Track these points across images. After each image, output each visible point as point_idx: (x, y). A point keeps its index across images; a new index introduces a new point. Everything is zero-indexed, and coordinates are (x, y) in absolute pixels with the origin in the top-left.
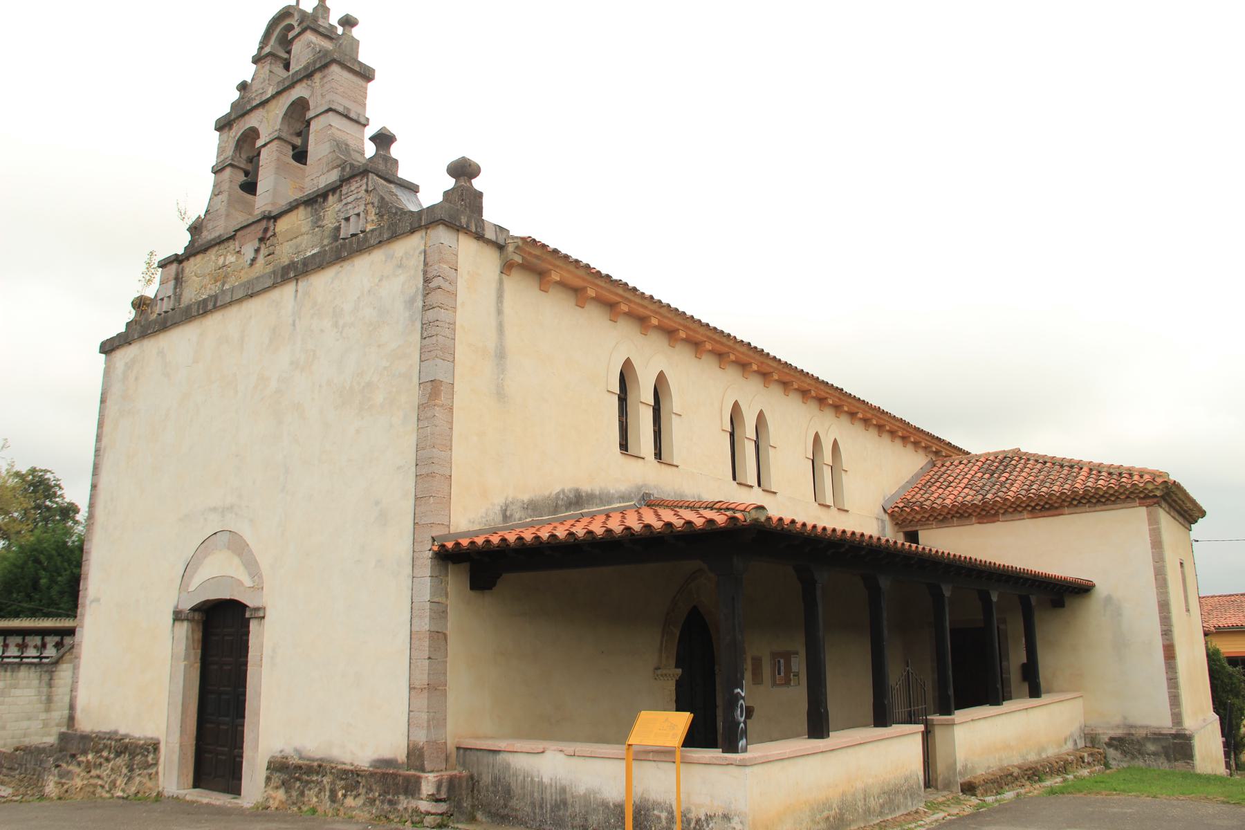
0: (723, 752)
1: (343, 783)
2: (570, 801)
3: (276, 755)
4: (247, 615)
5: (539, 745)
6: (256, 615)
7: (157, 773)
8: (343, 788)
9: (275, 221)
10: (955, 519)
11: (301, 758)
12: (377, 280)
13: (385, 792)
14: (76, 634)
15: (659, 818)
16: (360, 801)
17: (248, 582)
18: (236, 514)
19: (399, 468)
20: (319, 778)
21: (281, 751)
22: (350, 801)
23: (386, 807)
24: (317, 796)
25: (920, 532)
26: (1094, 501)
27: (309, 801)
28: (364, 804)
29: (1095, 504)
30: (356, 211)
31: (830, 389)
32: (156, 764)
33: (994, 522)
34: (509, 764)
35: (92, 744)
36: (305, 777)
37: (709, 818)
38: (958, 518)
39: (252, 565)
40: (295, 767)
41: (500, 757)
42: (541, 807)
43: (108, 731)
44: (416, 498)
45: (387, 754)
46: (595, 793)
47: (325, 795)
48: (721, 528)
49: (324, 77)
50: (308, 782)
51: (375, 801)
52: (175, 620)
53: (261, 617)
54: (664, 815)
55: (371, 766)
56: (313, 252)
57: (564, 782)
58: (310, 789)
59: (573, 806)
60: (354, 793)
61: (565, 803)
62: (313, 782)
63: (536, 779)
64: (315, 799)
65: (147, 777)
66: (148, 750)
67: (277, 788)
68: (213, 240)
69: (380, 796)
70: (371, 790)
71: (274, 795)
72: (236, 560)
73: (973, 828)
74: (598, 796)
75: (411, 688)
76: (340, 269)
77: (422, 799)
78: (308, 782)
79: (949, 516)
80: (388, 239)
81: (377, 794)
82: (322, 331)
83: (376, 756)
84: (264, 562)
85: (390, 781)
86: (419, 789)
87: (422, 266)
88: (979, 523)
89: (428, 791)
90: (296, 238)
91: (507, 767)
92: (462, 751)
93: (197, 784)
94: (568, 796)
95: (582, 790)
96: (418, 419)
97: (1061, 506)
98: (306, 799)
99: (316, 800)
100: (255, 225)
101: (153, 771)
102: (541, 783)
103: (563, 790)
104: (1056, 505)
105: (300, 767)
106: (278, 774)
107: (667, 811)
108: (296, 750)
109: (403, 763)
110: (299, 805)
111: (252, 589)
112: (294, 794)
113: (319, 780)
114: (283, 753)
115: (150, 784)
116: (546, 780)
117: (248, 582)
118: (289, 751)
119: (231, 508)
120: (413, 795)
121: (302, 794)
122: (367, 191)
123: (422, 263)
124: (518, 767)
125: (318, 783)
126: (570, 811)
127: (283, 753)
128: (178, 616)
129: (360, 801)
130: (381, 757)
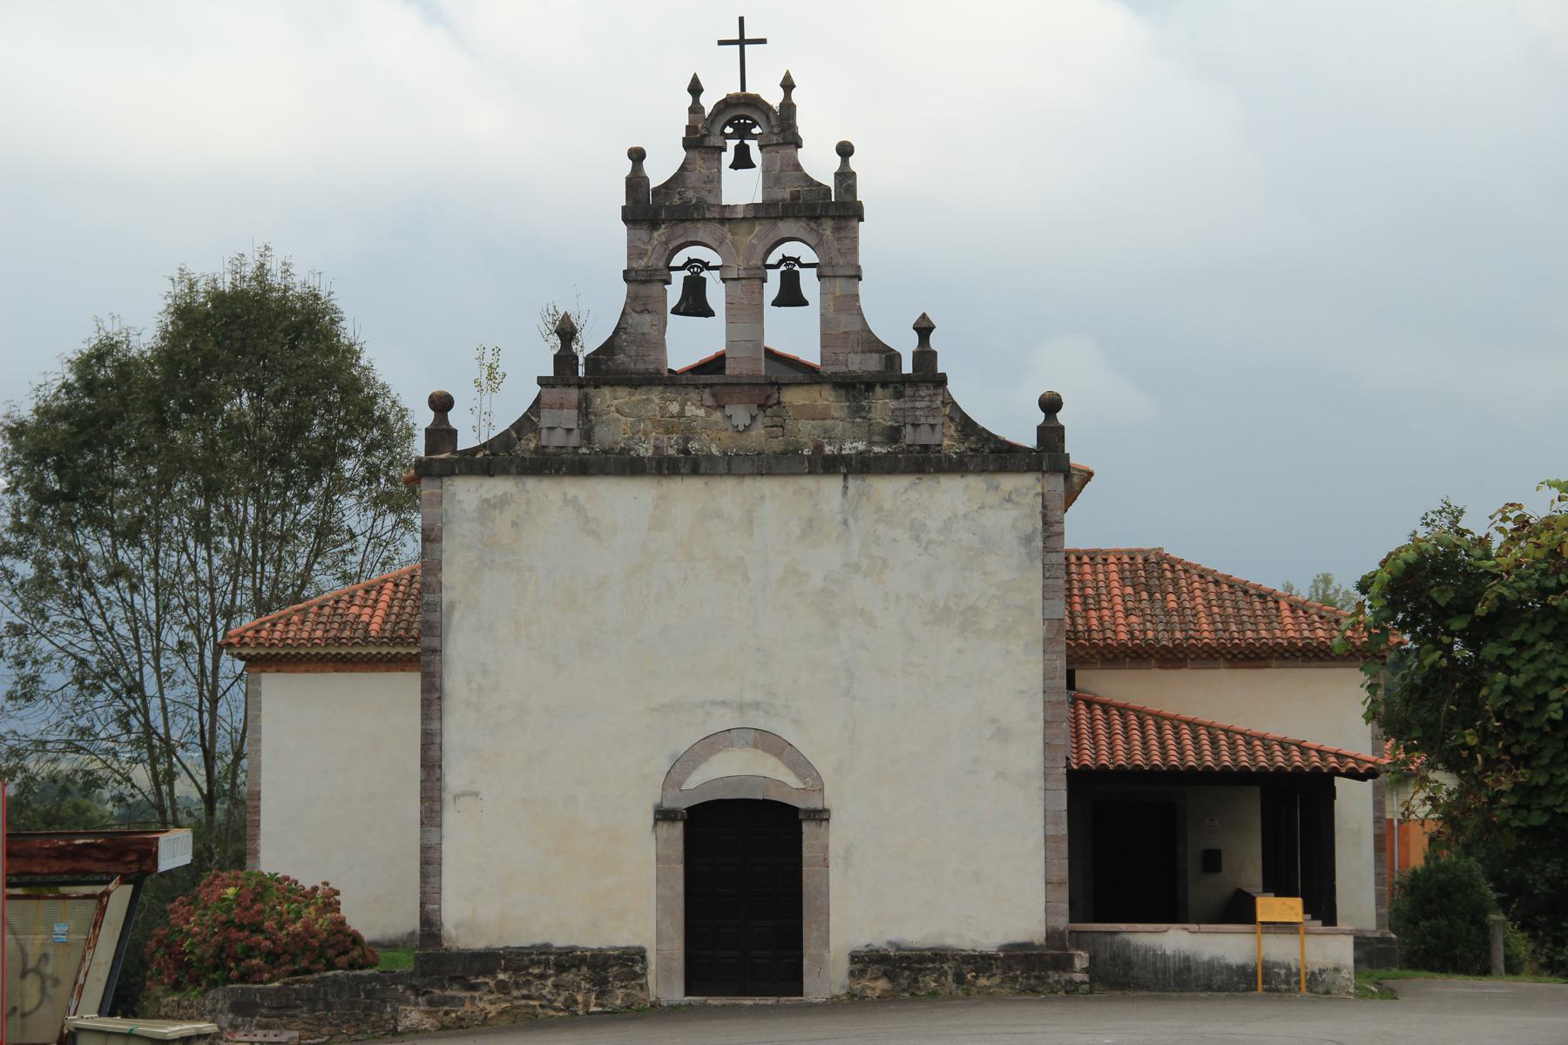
0: (1324, 925)
1: (971, 966)
4: (801, 817)
5: (1164, 926)
7: (647, 982)
9: (779, 389)
10: (1128, 659)
12: (976, 507)
14: (1224, 865)
15: (1279, 974)
17: (793, 781)
18: (767, 713)
19: (1022, 692)
21: (867, 946)
22: (983, 981)
25: (1077, 672)
26: (1311, 655)
28: (1003, 982)
29: (1310, 659)
30: (931, 421)
32: (644, 975)
33: (1180, 668)
35: (503, 962)
37: (1322, 971)
38: (1132, 658)
39: (799, 763)
41: (1118, 938)
42: (1164, 973)
44: (1046, 722)
46: (1218, 959)
50: (920, 970)
52: (656, 820)
53: (821, 816)
54: (1283, 972)
57: (1187, 953)
58: (925, 976)
59: (1196, 970)
61: (1188, 969)
62: (929, 969)
63: (1159, 952)
65: (638, 988)
66: (633, 961)
67: (876, 979)
78: (920, 970)
79: (1122, 655)
81: (1019, 972)
82: (895, 540)
83: (1006, 942)
87: (1039, 508)
88: (1160, 668)
90: (822, 419)
91: (1128, 943)
92: (1074, 934)
93: (687, 994)
95: (1206, 958)
96: (1044, 652)
97: (1269, 657)
98: (922, 985)
101: (643, 981)
102: (1164, 955)
103: (1187, 959)
104: (1263, 655)
105: (908, 958)
107: (1286, 968)
108: (890, 943)
115: (642, 995)
116: (1169, 952)
117: (793, 781)
119: (756, 705)
122: (943, 402)
123: (1040, 505)
128: (663, 815)
129: (996, 980)
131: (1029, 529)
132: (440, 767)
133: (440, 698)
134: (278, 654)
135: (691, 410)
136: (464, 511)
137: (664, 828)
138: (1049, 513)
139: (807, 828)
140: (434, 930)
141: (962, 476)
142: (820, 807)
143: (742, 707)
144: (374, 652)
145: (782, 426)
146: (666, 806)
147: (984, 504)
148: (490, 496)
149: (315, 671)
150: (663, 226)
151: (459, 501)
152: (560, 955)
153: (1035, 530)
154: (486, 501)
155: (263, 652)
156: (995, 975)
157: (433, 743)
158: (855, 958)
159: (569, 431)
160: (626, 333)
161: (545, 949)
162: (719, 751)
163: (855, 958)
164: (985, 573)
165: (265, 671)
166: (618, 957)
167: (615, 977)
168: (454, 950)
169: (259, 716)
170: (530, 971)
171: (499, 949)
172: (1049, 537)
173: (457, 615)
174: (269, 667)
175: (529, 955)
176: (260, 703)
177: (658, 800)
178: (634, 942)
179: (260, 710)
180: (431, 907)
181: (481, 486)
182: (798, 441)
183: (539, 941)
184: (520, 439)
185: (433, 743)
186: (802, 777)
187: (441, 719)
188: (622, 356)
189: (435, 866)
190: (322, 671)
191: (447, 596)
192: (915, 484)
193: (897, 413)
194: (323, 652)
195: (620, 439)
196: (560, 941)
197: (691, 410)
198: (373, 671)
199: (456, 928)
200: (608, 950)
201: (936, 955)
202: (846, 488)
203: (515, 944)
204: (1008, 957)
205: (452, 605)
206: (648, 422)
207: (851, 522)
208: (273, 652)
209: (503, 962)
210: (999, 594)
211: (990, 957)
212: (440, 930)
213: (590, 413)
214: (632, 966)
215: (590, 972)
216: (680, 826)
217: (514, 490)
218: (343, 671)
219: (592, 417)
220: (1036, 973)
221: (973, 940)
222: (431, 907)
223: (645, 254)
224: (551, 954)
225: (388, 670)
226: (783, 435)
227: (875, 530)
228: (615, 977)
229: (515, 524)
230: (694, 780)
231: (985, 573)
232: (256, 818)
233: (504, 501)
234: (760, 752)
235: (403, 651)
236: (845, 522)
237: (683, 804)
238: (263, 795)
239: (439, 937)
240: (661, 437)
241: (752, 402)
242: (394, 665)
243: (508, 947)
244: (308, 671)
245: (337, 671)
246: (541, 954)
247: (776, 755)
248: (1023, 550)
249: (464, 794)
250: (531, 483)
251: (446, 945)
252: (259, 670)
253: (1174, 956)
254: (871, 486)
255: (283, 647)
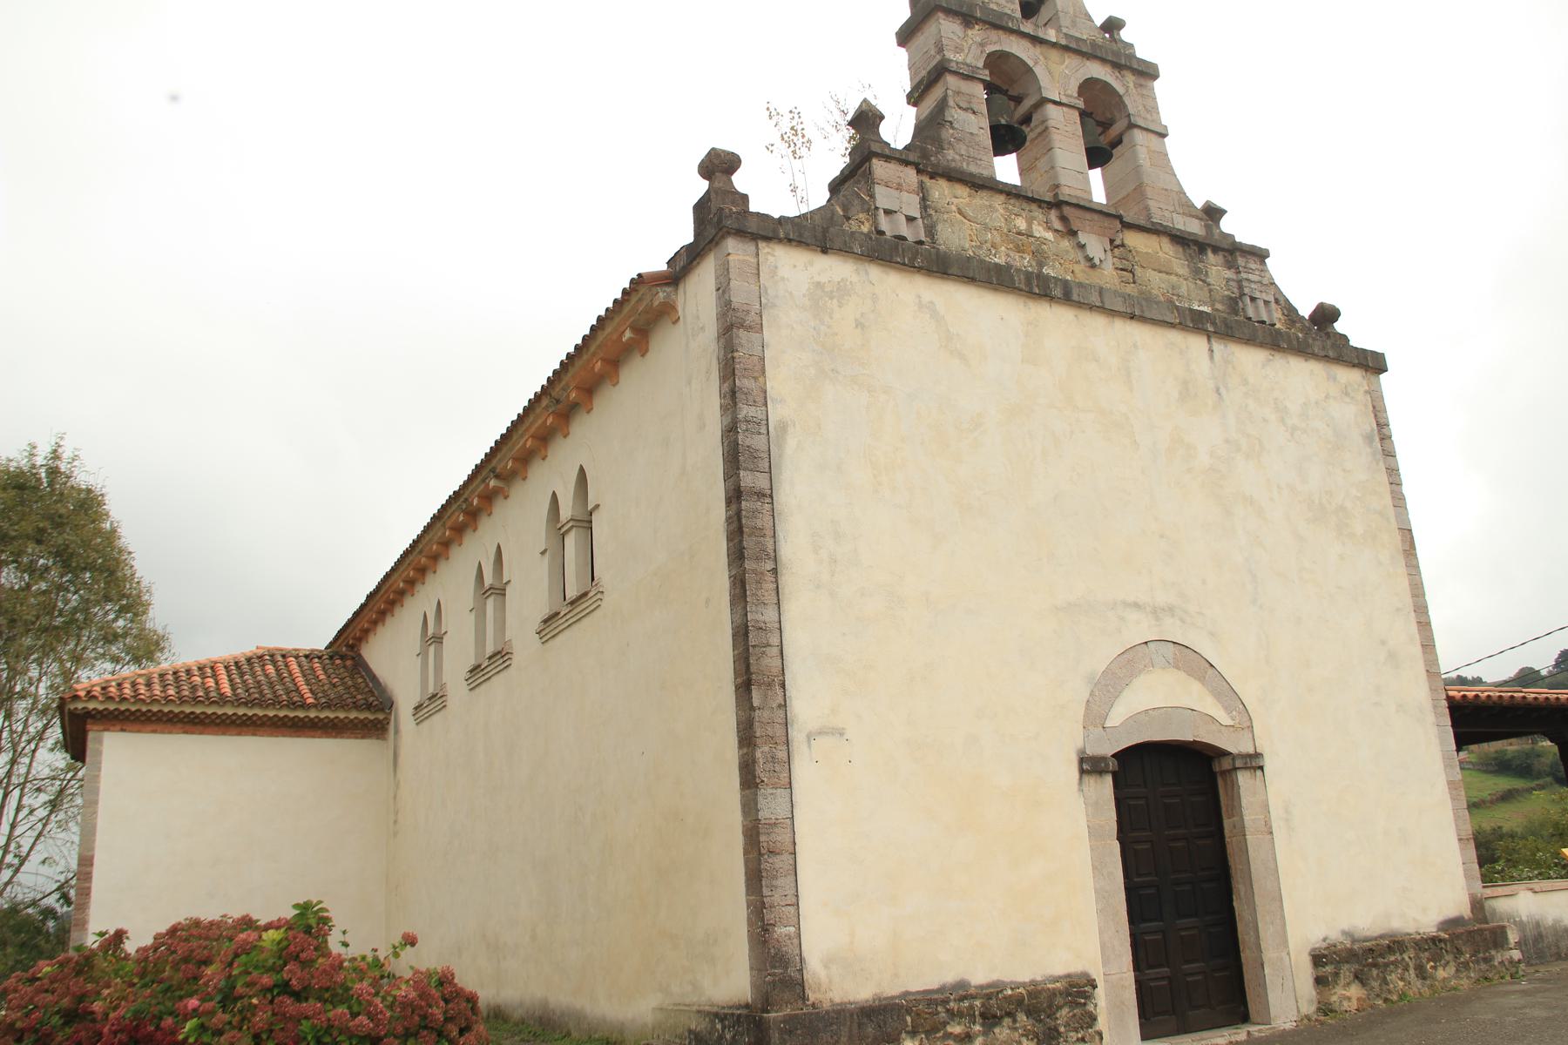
1: (1427, 954)
2: (1544, 933)
3: (1317, 946)
6: (1254, 764)
8: (1429, 960)
11: (1354, 941)
13: (1476, 952)
16: (1451, 970)
18: (1182, 621)
19: (1398, 610)
20: (1398, 956)
21: (1324, 940)
22: (1441, 973)
23: (1483, 966)
24: (1402, 979)
27: (1395, 987)
28: (1457, 971)
31: (415, 550)
34: (1494, 910)
35: (909, 1019)
36: (1380, 960)
39: (1227, 694)
40: (1364, 951)
42: (1526, 945)
43: (935, 986)
45: (1451, 912)
47: (1409, 974)
48: (1552, 705)
49: (1141, 85)
50: (1387, 965)
51: (1468, 964)
52: (1082, 772)
55: (1439, 930)
56: (1201, 308)
57: (1537, 917)
59: (1547, 937)
60: (1443, 962)
62: (1392, 963)
63: (1517, 919)
64: (1401, 984)
67: (1348, 984)
68: (971, 174)
69: (1471, 957)
70: (1459, 952)
71: (1348, 994)
72: (1196, 686)
73: (957, 1038)
74: (1562, 924)
75: (1460, 840)
76: (1271, 357)
77: (1511, 949)
80: (1333, 359)
83: (1441, 918)
84: (1248, 693)
85: (1477, 938)
86: (1507, 939)
89: (1514, 939)
90: (1167, 273)
94: (1542, 929)
99: (1403, 983)
100: (1101, 216)
105: (1371, 950)
106: (1346, 966)
108: (1344, 933)
109: (1470, 919)
110: (1384, 996)
111: (1232, 729)
112: (1375, 984)
113: (1399, 958)
114: (1328, 941)
118: (1335, 935)
119: (1171, 610)
120: (1502, 947)
121: (1384, 981)
124: (1502, 910)
125: (1395, 963)
126: (1546, 942)
127: (1328, 941)
130: (1446, 918)
131: (1368, 428)
132: (783, 686)
133: (775, 571)
134: (128, 710)
135: (1039, 231)
136: (791, 293)
137: (1091, 781)
138: (1378, 413)
139: (1243, 778)
140: (791, 972)
141: (1306, 360)
142: (1251, 751)
143: (1157, 612)
144: (230, 713)
145: (1131, 271)
146: (1090, 752)
147: (1328, 394)
148: (823, 279)
149: (162, 732)
150: (977, 27)
151: (783, 279)
152: (989, 997)
153: (1372, 430)
154: (818, 285)
155: (112, 707)
156: (1448, 962)
157: (768, 645)
158: (1318, 959)
159: (910, 219)
160: (953, 128)
161: (961, 990)
162: (1140, 672)
163: (1318, 959)
164: (1344, 470)
165: (107, 730)
166: (1066, 993)
167: (1067, 1025)
168: (826, 1006)
169: (98, 776)
170: (949, 1029)
171: (893, 998)
172: (1383, 439)
173: (791, 443)
174: (114, 725)
175: (945, 1002)
176: (100, 763)
177: (1080, 744)
178: (1075, 967)
179: (100, 771)
180: (784, 930)
181: (811, 264)
182: (1150, 293)
183: (950, 977)
184: (848, 219)
185: (768, 645)
186: (1228, 709)
187: (778, 603)
188: (951, 152)
189: (786, 857)
190: (170, 733)
191: (776, 413)
192: (1270, 360)
193: (1231, 283)
194: (177, 710)
195: (967, 246)
196: (979, 976)
197: (1039, 231)
198: (224, 734)
199: (826, 967)
200: (1044, 982)
201: (1394, 942)
202: (1211, 351)
203: (916, 986)
204: (1454, 937)
205: (783, 427)
206: (995, 233)
207: (1223, 390)
208: (123, 708)
209: (909, 1019)
210: (1359, 495)
211: (1434, 940)
212: (801, 970)
213: (930, 207)
214: (1085, 1004)
215: (1031, 1021)
216: (1109, 779)
217: (855, 278)
218: (193, 733)
219: (932, 212)
220: (1481, 955)
221: (1414, 920)
222: (784, 930)
223: (962, 50)
224: (974, 997)
225: (239, 734)
226: (1134, 282)
227: (1246, 406)
228: (1067, 1025)
229: (859, 325)
230: (1116, 717)
231: (1344, 470)
232: (87, 885)
233: (841, 291)
234: (1182, 675)
235: (261, 713)
236: (1218, 390)
237: (1109, 749)
238: (96, 861)
239: (802, 984)
240: (1012, 254)
241: (1104, 235)
242: (245, 729)
243: (907, 993)
244: (154, 731)
245: (186, 732)
246: (962, 999)
247: (1199, 680)
248: (1369, 450)
249: (821, 732)
250: (875, 272)
251: (812, 997)
252: (102, 728)
253: (1529, 922)
254: (1233, 353)
255: (134, 703)
